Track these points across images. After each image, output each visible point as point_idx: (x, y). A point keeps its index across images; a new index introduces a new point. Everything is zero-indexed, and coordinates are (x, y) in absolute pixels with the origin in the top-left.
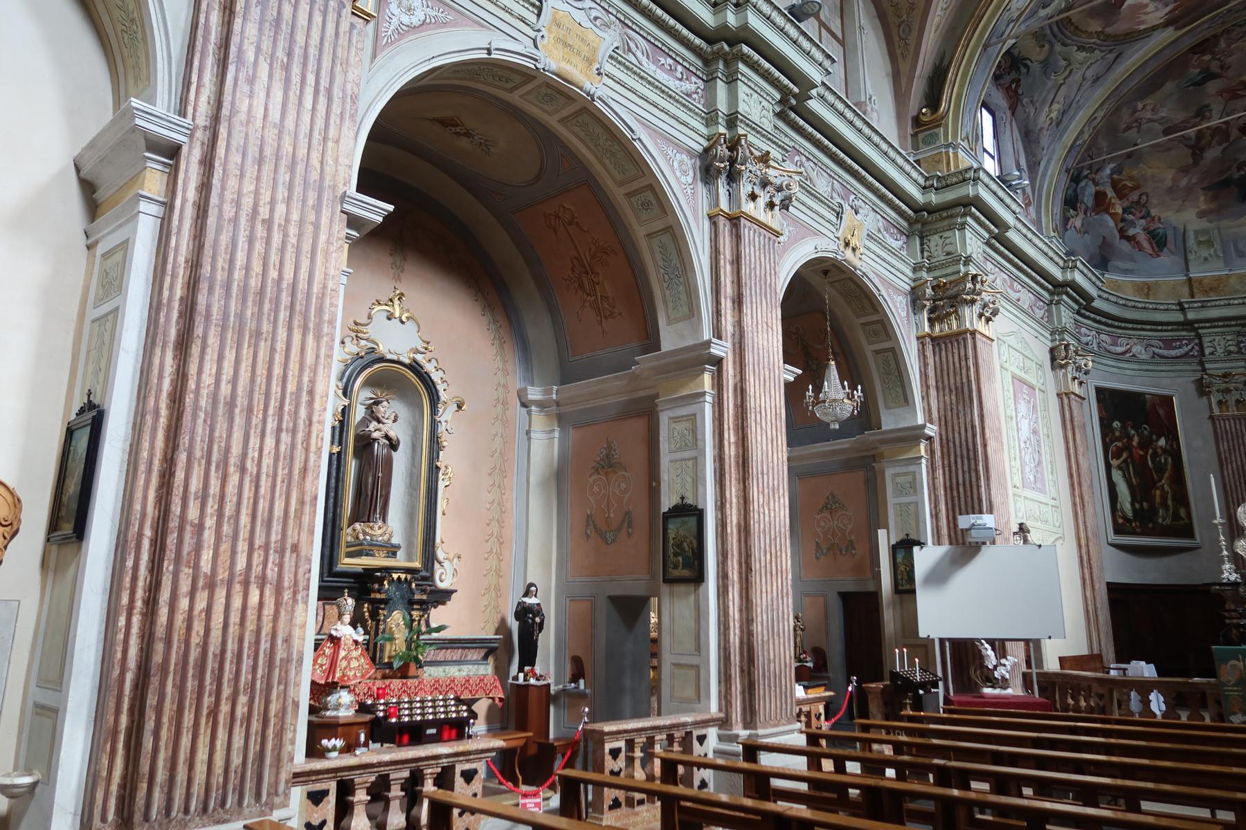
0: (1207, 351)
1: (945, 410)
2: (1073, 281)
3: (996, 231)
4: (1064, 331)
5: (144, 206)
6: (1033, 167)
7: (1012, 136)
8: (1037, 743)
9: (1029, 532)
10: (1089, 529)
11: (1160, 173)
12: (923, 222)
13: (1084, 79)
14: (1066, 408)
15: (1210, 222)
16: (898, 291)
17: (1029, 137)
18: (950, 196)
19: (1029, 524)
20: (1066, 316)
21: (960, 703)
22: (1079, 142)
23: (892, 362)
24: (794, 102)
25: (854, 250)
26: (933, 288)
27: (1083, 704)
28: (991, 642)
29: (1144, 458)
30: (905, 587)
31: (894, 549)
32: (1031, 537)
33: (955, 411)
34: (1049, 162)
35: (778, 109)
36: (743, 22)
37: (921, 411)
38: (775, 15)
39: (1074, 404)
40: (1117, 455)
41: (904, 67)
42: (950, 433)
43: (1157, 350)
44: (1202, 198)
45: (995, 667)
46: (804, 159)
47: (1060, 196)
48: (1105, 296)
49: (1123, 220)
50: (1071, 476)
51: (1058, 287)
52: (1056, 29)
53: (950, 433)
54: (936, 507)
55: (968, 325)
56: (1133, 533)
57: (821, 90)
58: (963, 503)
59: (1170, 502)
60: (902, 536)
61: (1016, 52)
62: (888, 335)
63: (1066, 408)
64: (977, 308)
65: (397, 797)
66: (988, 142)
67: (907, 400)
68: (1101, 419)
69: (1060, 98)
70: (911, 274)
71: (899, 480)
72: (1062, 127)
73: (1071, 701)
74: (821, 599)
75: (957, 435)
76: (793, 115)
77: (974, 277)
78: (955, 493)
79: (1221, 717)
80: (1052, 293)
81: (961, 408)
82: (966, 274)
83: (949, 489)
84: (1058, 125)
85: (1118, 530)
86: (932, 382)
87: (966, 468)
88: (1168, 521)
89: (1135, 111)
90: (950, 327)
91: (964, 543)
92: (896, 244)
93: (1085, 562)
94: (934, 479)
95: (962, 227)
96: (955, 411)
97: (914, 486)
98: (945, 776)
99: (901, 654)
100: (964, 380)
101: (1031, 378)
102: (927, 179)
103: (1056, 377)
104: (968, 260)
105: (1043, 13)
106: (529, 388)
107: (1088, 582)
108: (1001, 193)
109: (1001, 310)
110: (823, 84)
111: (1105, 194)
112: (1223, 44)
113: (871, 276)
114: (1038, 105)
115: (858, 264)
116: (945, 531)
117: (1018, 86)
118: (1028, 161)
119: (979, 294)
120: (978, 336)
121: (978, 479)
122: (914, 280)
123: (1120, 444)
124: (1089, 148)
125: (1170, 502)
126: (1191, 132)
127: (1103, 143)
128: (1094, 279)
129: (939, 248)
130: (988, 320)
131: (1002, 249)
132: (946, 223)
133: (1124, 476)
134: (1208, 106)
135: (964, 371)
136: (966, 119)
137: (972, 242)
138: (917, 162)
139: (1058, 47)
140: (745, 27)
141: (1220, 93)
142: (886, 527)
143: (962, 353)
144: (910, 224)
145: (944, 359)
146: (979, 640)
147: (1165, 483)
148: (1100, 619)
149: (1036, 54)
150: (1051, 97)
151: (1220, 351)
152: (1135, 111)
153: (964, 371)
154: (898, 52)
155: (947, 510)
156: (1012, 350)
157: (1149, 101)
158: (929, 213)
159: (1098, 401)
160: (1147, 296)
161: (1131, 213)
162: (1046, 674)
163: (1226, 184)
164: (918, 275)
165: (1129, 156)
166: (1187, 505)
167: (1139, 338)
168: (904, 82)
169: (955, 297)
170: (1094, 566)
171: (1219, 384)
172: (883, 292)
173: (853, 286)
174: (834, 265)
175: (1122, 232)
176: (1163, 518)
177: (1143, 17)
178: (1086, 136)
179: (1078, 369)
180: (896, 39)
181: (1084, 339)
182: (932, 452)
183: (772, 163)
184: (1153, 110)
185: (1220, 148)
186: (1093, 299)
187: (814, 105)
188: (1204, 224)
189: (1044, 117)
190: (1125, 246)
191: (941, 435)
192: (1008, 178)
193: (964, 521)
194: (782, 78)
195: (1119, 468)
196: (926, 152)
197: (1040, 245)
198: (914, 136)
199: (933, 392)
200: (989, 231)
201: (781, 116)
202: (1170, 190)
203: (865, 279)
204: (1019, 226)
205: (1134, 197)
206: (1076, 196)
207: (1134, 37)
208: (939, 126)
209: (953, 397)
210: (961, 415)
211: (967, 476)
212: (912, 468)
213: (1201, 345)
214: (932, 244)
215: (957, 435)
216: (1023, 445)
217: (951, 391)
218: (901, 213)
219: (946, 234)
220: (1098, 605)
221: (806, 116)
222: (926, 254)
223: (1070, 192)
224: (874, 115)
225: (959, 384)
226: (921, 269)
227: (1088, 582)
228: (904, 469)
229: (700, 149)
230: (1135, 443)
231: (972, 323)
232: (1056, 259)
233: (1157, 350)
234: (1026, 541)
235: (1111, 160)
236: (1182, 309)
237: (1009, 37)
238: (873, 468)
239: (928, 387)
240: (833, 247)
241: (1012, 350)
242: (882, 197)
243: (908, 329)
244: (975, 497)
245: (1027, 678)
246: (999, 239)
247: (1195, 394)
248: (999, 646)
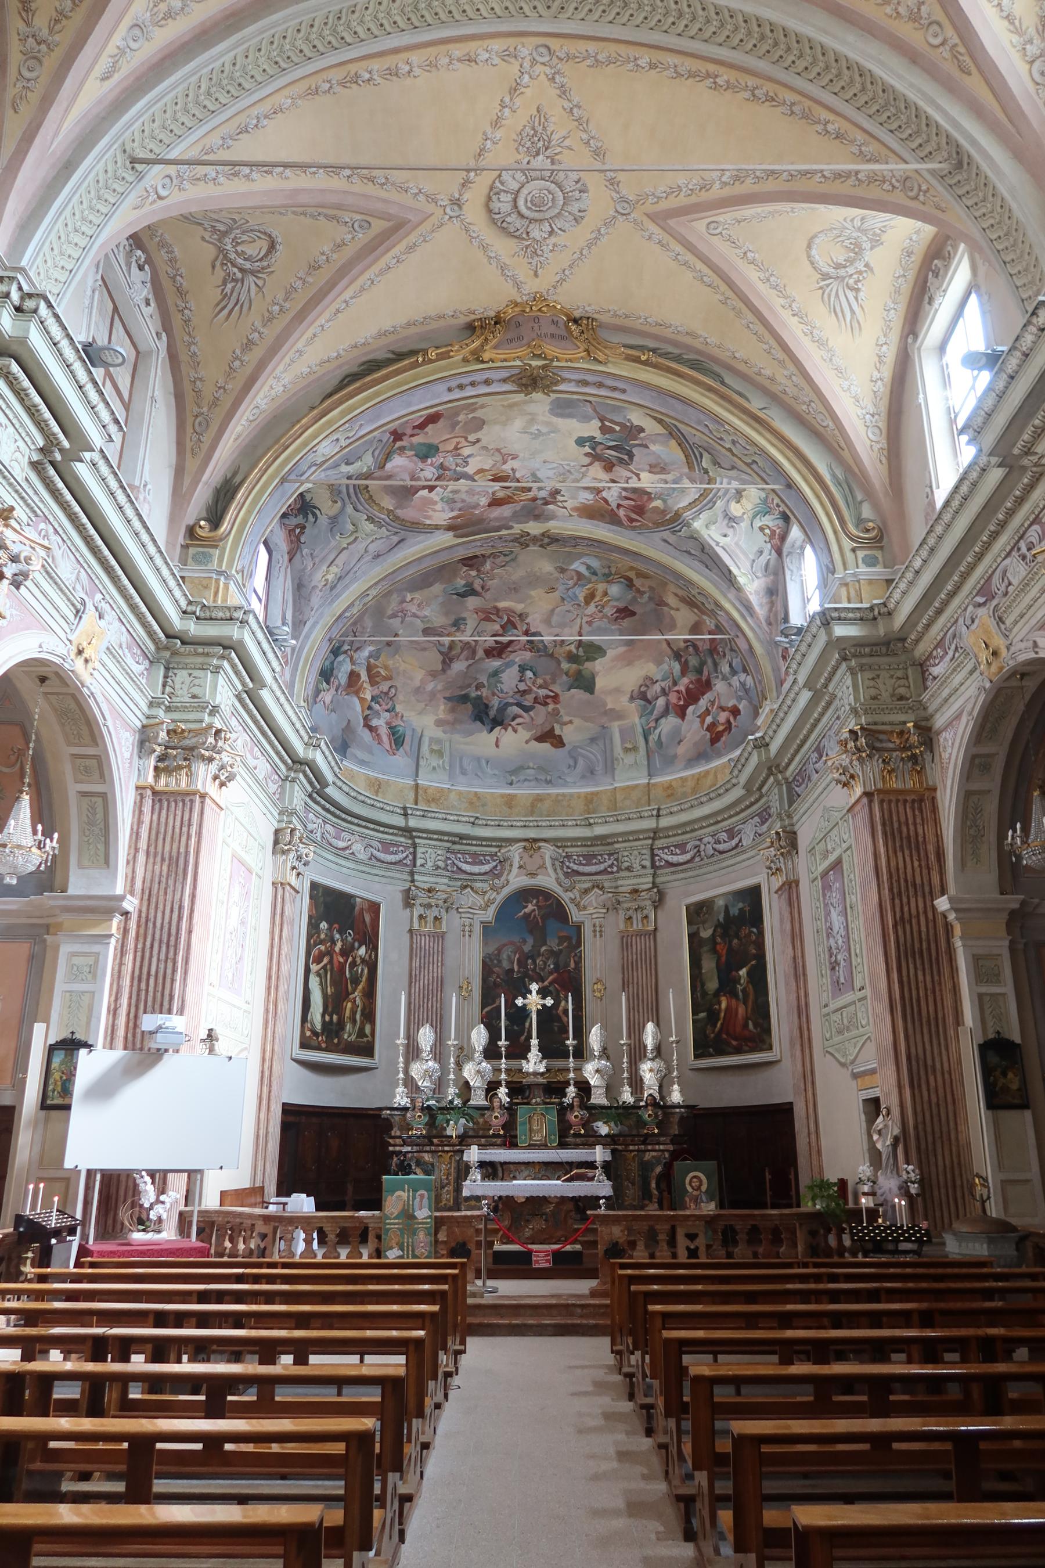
0: (419, 862)
1: (152, 881)
2: (314, 761)
3: (251, 685)
4: (293, 813)
6: (298, 624)
7: (284, 584)
8: (203, 1297)
9: (217, 1040)
10: (277, 1041)
11: (412, 670)
12: (173, 650)
13: (366, 551)
14: (279, 900)
15: (444, 732)
16: (127, 725)
17: (300, 589)
18: (211, 631)
19: (219, 1031)
20: (298, 797)
21: (102, 1254)
22: (347, 614)
24: (58, 457)
25: (86, 661)
26: (168, 732)
27: (241, 1246)
28: (152, 1174)
29: (342, 967)
30: (56, 1103)
31: (52, 1049)
32: (219, 1046)
33: (163, 885)
34: (316, 623)
35: (35, 457)
36: (21, 334)
37: (122, 879)
38: (64, 344)
39: (287, 896)
40: (318, 960)
41: (191, 464)
43: (375, 852)
44: (442, 707)
45: (151, 1207)
46: (51, 530)
47: (318, 666)
48: (340, 783)
49: (370, 708)
50: (269, 978)
51: (298, 763)
52: (351, 490)
54: (116, 1000)
55: (200, 787)
56: (318, 1048)
57: (96, 456)
58: (150, 999)
59: (358, 1017)
60: (65, 1034)
61: (308, 497)
62: (102, 775)
63: (279, 900)
64: (213, 768)
66: (259, 581)
67: (107, 861)
68: (310, 917)
69: (340, 561)
70: (145, 708)
71: (76, 960)
72: (335, 592)
73: (228, 1244)
75: (159, 915)
76: (52, 472)
77: (218, 732)
78: (143, 986)
79: (379, 1253)
80: (289, 769)
81: (171, 882)
82: (210, 726)
83: (138, 979)
84: (332, 589)
85: (304, 1045)
86: (143, 844)
87: (163, 957)
88: (353, 1038)
89: (403, 601)
90: (178, 782)
91: (141, 1049)
92: (138, 669)
93: (266, 1079)
94: (121, 964)
95: (217, 670)
96: (163, 885)
97: (94, 971)
98: (98, 1349)
99: (36, 1191)
100: (182, 850)
101: (250, 860)
102: (190, 603)
103: (274, 863)
104: (214, 711)
105: (345, 469)
107: (264, 1102)
108: (265, 646)
109: (238, 777)
110: (102, 451)
111: (359, 676)
112: (488, 566)
113: (100, 699)
114: (317, 560)
115: (88, 680)
116: (121, 1032)
117: (302, 533)
118: (293, 616)
119: (219, 752)
120: (208, 800)
121: (174, 971)
122: (148, 718)
123: (323, 948)
124: (355, 623)
125: (358, 1017)
126: (446, 640)
127: (368, 623)
128: (333, 763)
129: (185, 687)
130: (222, 784)
131: (251, 706)
132: (199, 660)
133: (321, 984)
134: (464, 619)
135: (184, 838)
136: (246, 549)
137: (223, 690)
138: (182, 578)
139: (349, 509)
140: (23, 341)
141: (477, 611)
142: (47, 1020)
143: (186, 818)
144: (158, 648)
145: (163, 820)
146: (139, 1172)
147: (357, 995)
148: (270, 1145)
149: (327, 507)
150: (332, 557)
151: (430, 864)
152: (403, 601)
153: (184, 838)
154: (189, 445)
155: (129, 1005)
156: (239, 826)
157: (417, 595)
158: (183, 643)
159: (311, 897)
160: (377, 793)
161: (378, 703)
162: (206, 1212)
163: (464, 699)
164: (154, 712)
165: (389, 644)
166: (373, 1023)
167: (363, 837)
168: (187, 481)
169: (192, 749)
170: (274, 1083)
171: (423, 898)
172: (109, 723)
173: (73, 706)
174: (57, 674)
175: (366, 718)
176: (349, 1034)
177: (431, 513)
178: (355, 610)
179: (299, 858)
180: (189, 430)
181: (310, 826)
182: (126, 931)
183: (12, 522)
184: (419, 605)
185: (466, 664)
186: (327, 785)
187: (82, 470)
188: (439, 733)
189: (321, 576)
190: (366, 735)
191: (140, 912)
192: (276, 631)
193: (149, 1022)
194: (53, 423)
195: (318, 974)
196: (194, 571)
197: (291, 713)
198: (185, 547)
199: (141, 857)
200: (244, 684)
201: (35, 465)
202: (418, 691)
203: (91, 701)
204: (275, 687)
205: (384, 687)
206: (332, 670)
207: (417, 527)
208: (216, 547)
209: (165, 868)
210: (170, 891)
211: (162, 966)
212: (96, 948)
213: (414, 854)
214: (178, 680)
215: (159, 915)
216: (228, 936)
217: (163, 860)
218: (151, 634)
219: (196, 673)
220: (271, 1130)
221: (68, 478)
222: (168, 689)
223: (327, 663)
224: (147, 506)
225: (174, 854)
226: (159, 705)
227: (264, 1102)
228: (86, 948)
230: (337, 949)
231: (204, 784)
232: (302, 732)
233: (375, 852)
234: (211, 1051)
235: (372, 642)
236: (406, 815)
237: (307, 480)
238: (45, 941)
239: (137, 850)
240: (62, 650)
241: (239, 826)
242: (133, 608)
243: (128, 772)
244: (167, 992)
245: (184, 1220)
246: (250, 697)
247: (401, 904)
248: (160, 1178)
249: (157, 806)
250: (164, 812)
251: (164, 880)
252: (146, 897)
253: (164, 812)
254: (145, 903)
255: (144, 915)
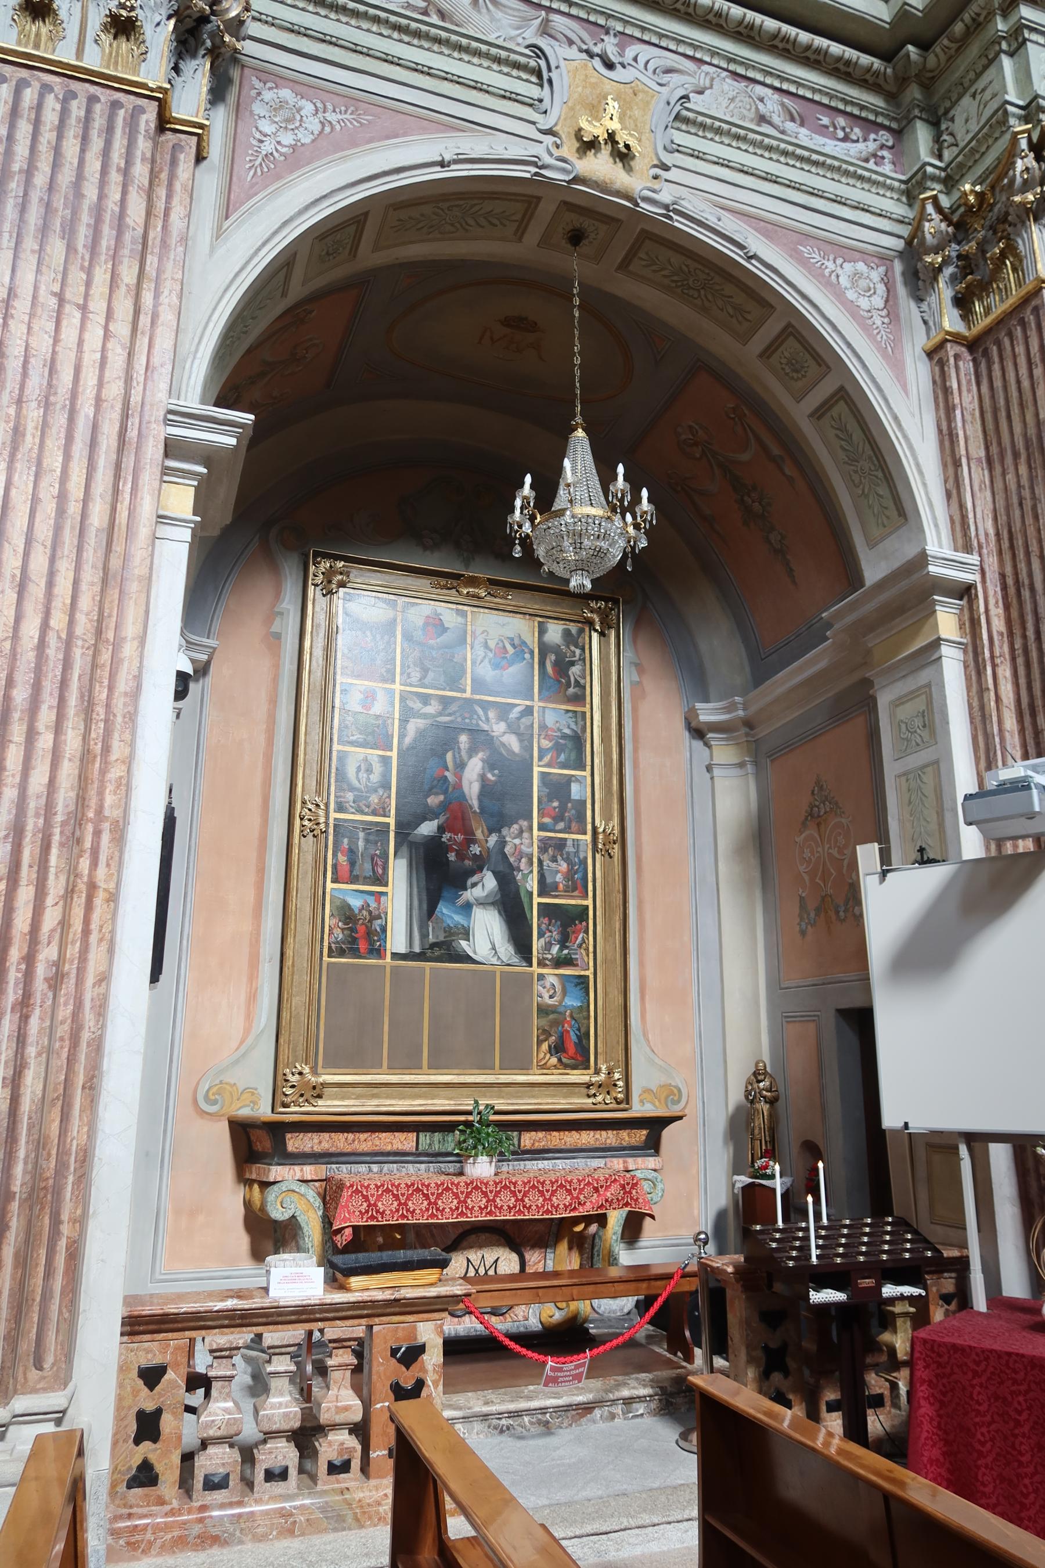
1: (1008, 507)
5: (945, 650)
23: (852, 425)
42: (1022, 566)
53: (1022, 566)
65: (906, 1314)
74: (812, 1026)
92: (851, 151)
106: (698, 705)
132: (974, 50)
144: (891, 97)
145: (998, 383)
173: (677, 260)
209: (1023, 469)
217: (1016, 455)
229: (899, 244)
249: (983, 366)
250: (996, 367)
251: (1026, 493)
252: (1006, 544)
253: (996, 367)
254: (1007, 557)
255: (1010, 581)
